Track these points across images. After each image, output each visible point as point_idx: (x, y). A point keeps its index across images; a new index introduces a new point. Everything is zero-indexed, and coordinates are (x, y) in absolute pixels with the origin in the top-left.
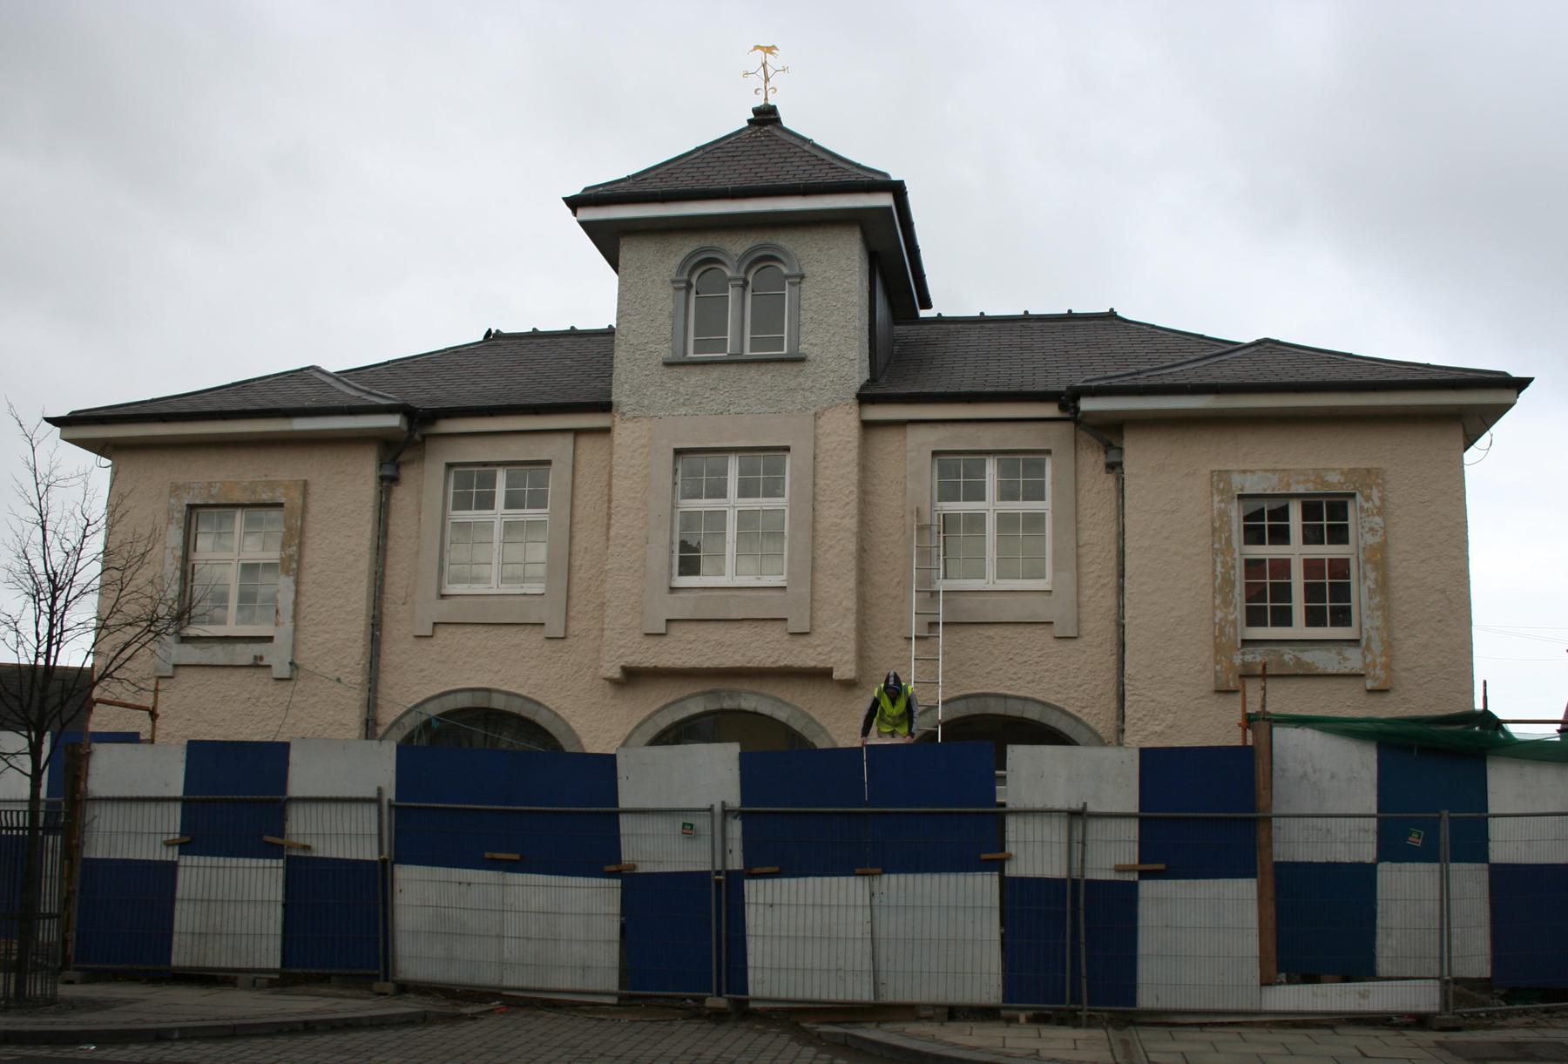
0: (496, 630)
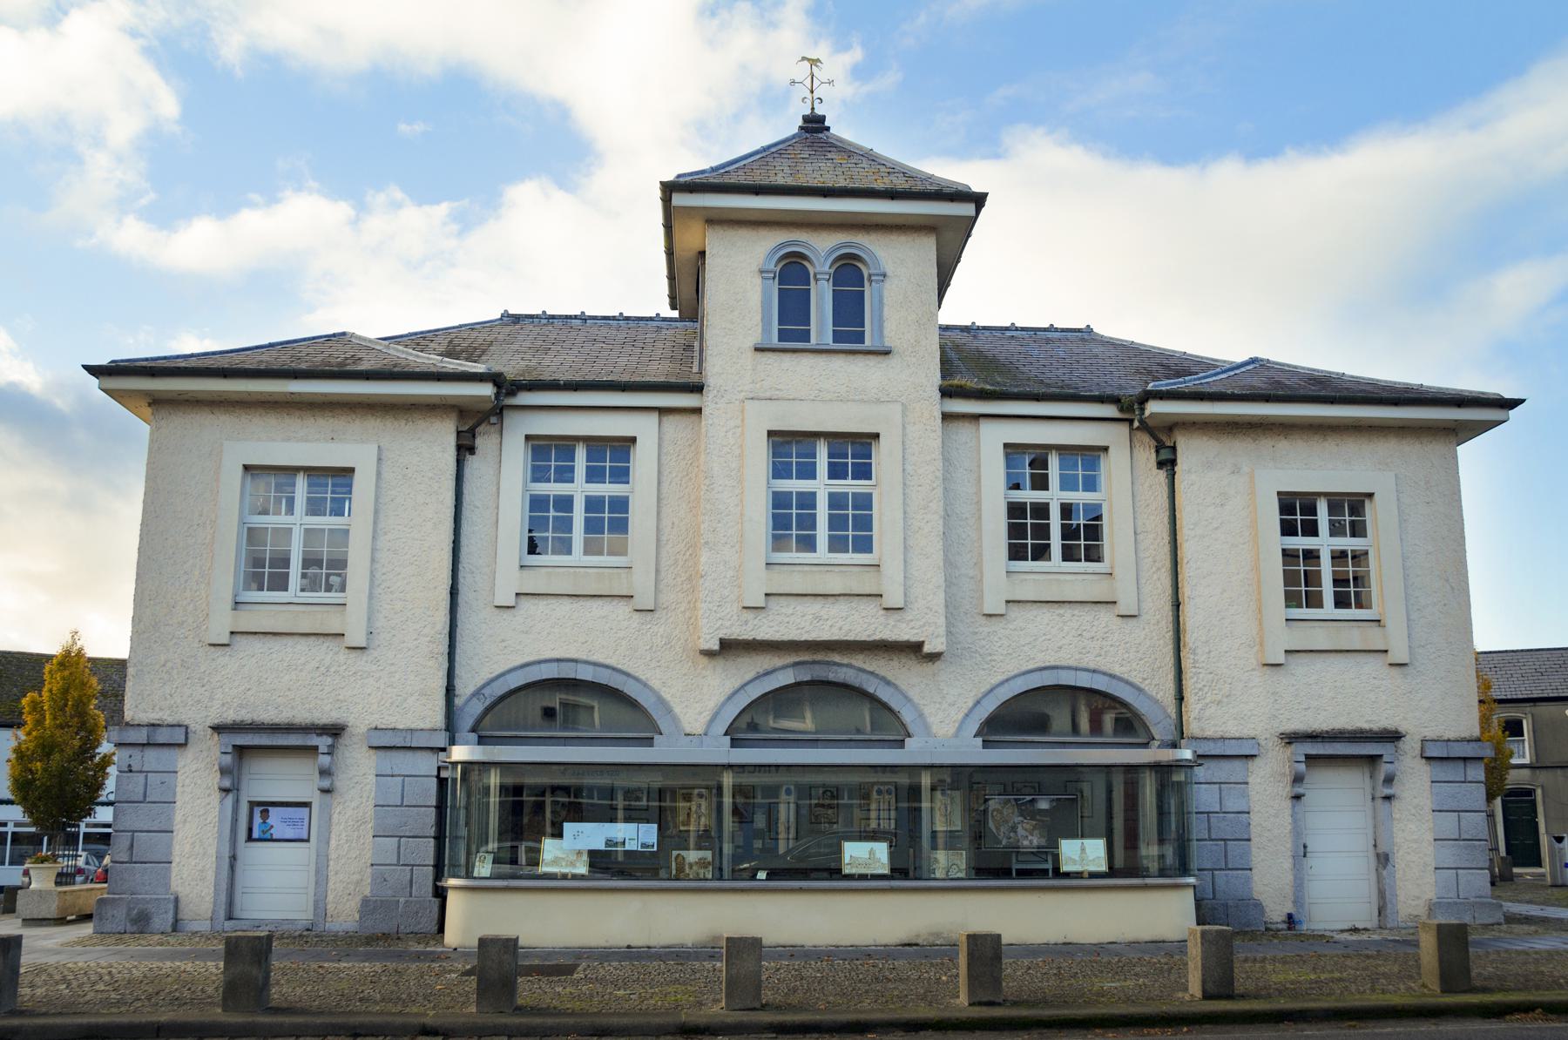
0: (582, 602)
